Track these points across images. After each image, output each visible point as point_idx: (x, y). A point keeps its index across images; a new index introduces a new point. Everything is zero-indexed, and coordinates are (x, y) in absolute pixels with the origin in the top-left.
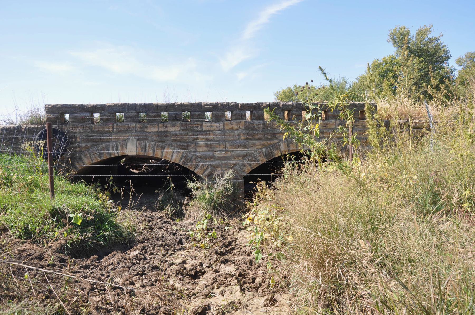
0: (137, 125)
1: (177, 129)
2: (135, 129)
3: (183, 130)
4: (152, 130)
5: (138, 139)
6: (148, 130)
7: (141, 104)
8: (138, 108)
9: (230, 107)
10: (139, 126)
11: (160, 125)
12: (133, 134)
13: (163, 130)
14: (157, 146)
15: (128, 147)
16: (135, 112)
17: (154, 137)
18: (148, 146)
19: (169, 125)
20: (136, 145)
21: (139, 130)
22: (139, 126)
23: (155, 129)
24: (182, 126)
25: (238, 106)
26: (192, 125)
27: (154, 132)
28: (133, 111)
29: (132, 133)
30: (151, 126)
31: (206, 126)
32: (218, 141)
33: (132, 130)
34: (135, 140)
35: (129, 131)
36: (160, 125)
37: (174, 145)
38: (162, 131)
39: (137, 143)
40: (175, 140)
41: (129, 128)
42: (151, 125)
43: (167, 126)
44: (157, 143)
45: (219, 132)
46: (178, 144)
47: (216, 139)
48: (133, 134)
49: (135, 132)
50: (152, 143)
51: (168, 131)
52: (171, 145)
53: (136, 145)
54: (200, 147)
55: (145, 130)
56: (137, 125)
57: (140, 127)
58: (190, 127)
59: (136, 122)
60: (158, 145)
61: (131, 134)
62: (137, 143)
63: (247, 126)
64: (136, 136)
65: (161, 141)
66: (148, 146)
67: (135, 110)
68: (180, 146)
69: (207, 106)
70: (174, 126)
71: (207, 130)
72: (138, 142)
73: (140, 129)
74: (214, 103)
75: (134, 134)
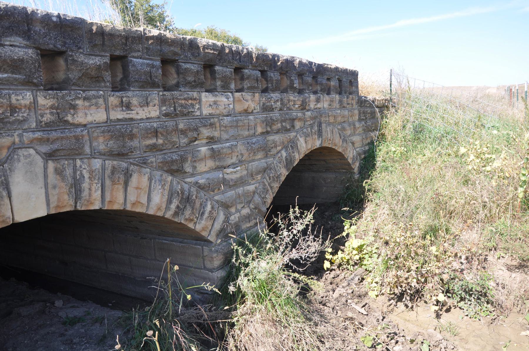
0: (41, 101)
1: (154, 112)
2: (32, 114)
3: (166, 115)
4: (90, 119)
5: (50, 156)
6: (80, 118)
7: (47, 17)
8: (38, 28)
9: (242, 59)
10: (49, 102)
11: (111, 99)
12: (28, 136)
13: (120, 117)
14: (113, 173)
15: (15, 190)
16: (27, 47)
17: (101, 144)
18: (86, 175)
19: (135, 101)
20: (46, 176)
21: (48, 117)
22: (49, 102)
23: (100, 116)
24: (163, 102)
25: (252, 56)
26: (185, 99)
27: (98, 125)
28: (18, 40)
29: (25, 131)
30: (87, 104)
31: (208, 103)
32: (227, 140)
33: (25, 120)
34: (39, 161)
35: (12, 123)
36: (113, 100)
37: (152, 162)
38: (119, 120)
39: (45, 169)
40: (153, 148)
41: (13, 109)
42: (85, 99)
43: (129, 103)
44: (109, 164)
45: (229, 118)
46: (160, 158)
47: (225, 136)
48: (28, 136)
49: (34, 125)
50: (97, 163)
51: (132, 119)
52: (144, 163)
53: (46, 176)
54: (201, 160)
55: (69, 118)
56: (41, 101)
57: (52, 107)
58: (182, 106)
59: (36, 85)
60: (114, 167)
61: (20, 136)
62: (45, 169)
63: (264, 104)
64: (41, 141)
65: (121, 155)
66: (86, 175)
67: (27, 35)
68: (164, 163)
69: (209, 51)
70: (148, 104)
71: (210, 114)
72: (51, 165)
73: (52, 113)
74: (333, 67)
75: (31, 135)
